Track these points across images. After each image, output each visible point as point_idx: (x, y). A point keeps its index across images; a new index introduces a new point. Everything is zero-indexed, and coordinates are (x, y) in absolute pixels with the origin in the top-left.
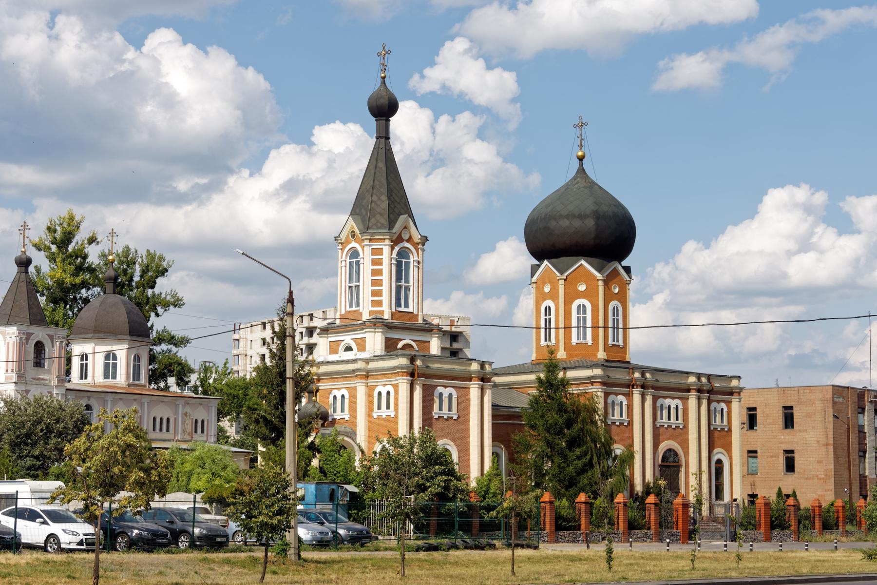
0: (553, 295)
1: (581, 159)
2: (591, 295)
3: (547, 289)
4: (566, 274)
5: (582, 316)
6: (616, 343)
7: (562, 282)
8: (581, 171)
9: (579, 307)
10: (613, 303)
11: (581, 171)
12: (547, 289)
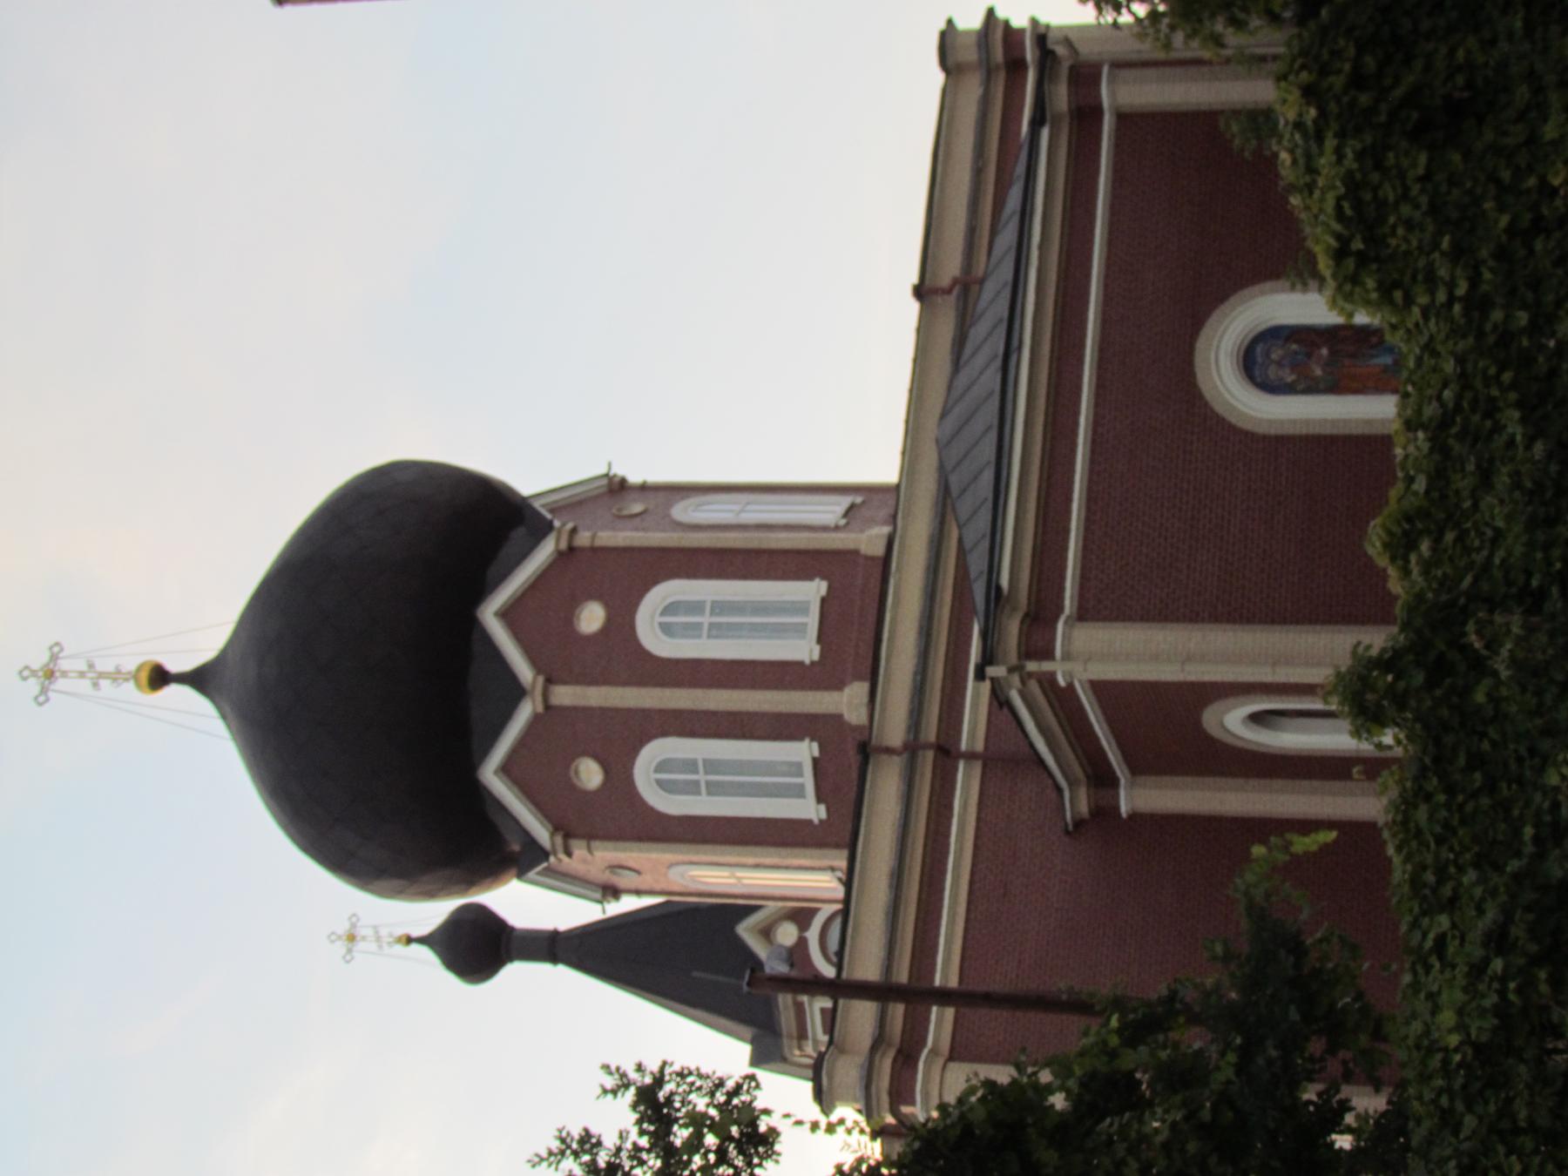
1: (159, 677)
2: (620, 738)
4: (523, 670)
6: (812, 620)
7: (565, 695)
8: (199, 679)
10: (652, 636)
11: (199, 679)
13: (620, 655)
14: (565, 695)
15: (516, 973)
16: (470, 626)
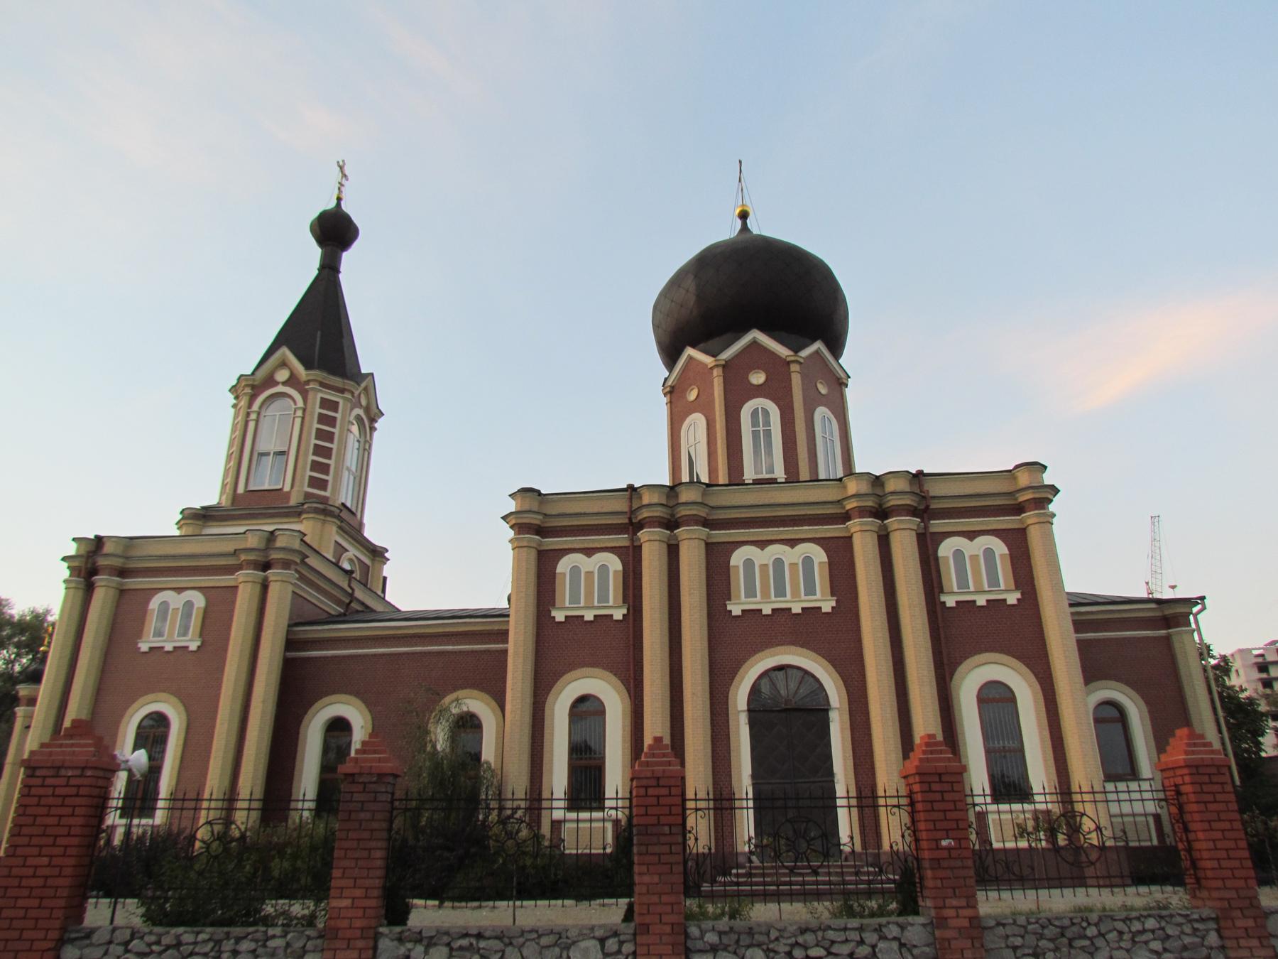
0: (702, 404)
2: (778, 391)
3: (692, 395)
5: (761, 428)
9: (755, 413)
12: (692, 395)
13: (737, 393)
14: (794, 367)
15: (313, 254)
16: (746, 330)
